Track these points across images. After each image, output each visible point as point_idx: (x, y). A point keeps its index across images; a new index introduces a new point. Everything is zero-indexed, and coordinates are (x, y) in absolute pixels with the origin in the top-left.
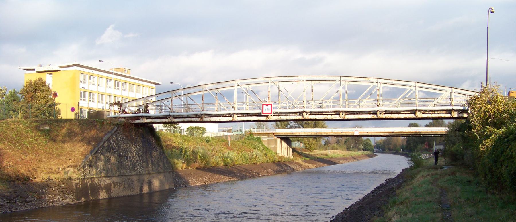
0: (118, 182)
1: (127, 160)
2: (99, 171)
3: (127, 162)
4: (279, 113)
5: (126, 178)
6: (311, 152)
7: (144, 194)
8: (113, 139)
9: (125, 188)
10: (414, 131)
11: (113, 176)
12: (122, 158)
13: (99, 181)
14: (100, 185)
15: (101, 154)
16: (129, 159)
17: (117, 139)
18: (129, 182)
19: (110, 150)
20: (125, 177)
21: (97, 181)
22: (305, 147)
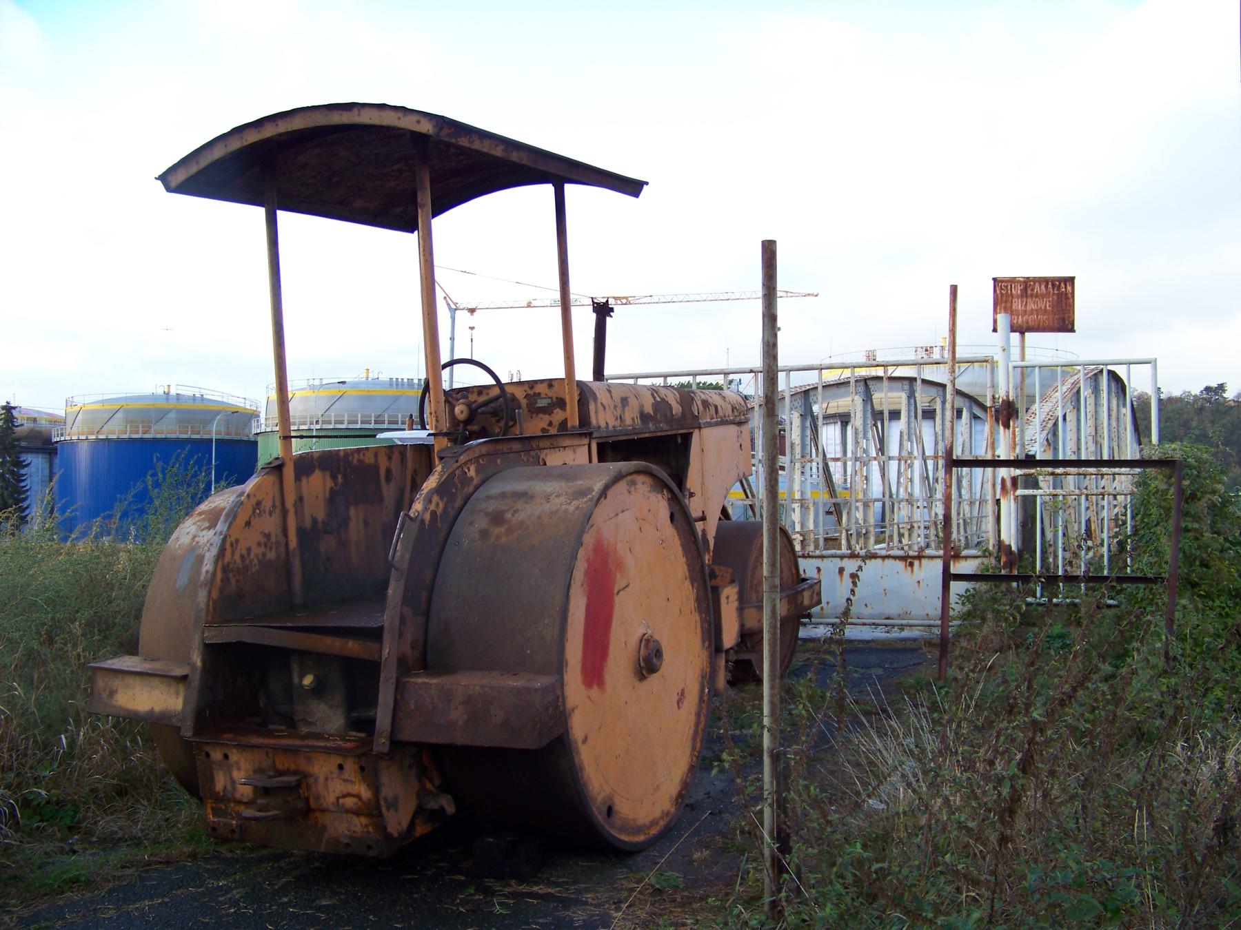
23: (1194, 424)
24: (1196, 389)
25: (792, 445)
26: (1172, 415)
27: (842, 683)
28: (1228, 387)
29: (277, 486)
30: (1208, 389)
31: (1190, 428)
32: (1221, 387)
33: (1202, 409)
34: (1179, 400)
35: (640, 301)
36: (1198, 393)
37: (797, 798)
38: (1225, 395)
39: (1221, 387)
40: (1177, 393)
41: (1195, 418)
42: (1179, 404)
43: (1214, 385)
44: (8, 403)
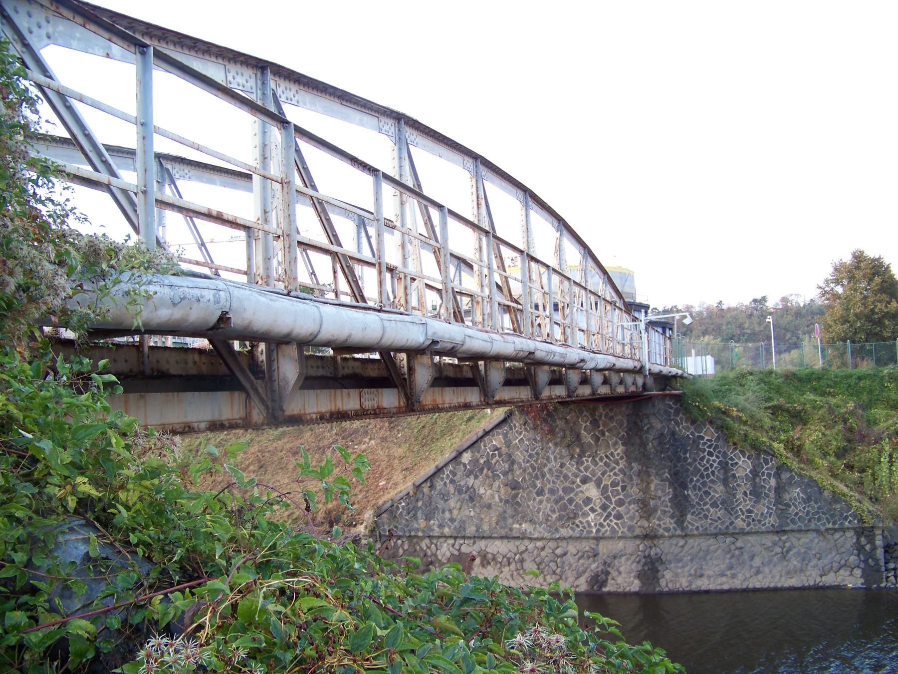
0: (498, 552)
1: (538, 499)
2: (437, 522)
3: (541, 502)
4: (699, 318)
5: (531, 546)
6: (872, 502)
7: (661, 594)
8: (494, 443)
9: (521, 572)
10: (525, 348)
11: (808, 530)
12: (521, 491)
13: (433, 546)
14: (435, 555)
15: (448, 481)
16: (547, 495)
17: (508, 444)
18: (540, 555)
19: (481, 470)
20: (526, 542)
21: (429, 545)
22: (537, 479)
23: (746, 326)
24: (746, 301)
25: (17, 43)
26: (730, 320)
27: (361, 529)
28: (768, 299)
29: (524, 218)
30: (755, 301)
31: (743, 329)
32: (764, 299)
33: (751, 315)
34: (736, 309)
35: (615, 333)
36: (748, 304)
37: (89, 312)
38: (766, 304)
39: (764, 299)
40: (733, 305)
41: (747, 322)
42: (735, 312)
43: (759, 297)
44: (880, 258)
